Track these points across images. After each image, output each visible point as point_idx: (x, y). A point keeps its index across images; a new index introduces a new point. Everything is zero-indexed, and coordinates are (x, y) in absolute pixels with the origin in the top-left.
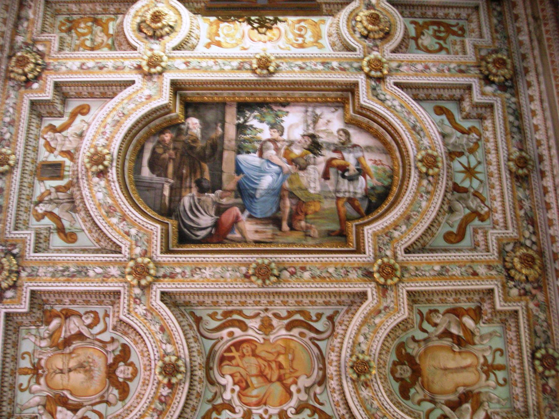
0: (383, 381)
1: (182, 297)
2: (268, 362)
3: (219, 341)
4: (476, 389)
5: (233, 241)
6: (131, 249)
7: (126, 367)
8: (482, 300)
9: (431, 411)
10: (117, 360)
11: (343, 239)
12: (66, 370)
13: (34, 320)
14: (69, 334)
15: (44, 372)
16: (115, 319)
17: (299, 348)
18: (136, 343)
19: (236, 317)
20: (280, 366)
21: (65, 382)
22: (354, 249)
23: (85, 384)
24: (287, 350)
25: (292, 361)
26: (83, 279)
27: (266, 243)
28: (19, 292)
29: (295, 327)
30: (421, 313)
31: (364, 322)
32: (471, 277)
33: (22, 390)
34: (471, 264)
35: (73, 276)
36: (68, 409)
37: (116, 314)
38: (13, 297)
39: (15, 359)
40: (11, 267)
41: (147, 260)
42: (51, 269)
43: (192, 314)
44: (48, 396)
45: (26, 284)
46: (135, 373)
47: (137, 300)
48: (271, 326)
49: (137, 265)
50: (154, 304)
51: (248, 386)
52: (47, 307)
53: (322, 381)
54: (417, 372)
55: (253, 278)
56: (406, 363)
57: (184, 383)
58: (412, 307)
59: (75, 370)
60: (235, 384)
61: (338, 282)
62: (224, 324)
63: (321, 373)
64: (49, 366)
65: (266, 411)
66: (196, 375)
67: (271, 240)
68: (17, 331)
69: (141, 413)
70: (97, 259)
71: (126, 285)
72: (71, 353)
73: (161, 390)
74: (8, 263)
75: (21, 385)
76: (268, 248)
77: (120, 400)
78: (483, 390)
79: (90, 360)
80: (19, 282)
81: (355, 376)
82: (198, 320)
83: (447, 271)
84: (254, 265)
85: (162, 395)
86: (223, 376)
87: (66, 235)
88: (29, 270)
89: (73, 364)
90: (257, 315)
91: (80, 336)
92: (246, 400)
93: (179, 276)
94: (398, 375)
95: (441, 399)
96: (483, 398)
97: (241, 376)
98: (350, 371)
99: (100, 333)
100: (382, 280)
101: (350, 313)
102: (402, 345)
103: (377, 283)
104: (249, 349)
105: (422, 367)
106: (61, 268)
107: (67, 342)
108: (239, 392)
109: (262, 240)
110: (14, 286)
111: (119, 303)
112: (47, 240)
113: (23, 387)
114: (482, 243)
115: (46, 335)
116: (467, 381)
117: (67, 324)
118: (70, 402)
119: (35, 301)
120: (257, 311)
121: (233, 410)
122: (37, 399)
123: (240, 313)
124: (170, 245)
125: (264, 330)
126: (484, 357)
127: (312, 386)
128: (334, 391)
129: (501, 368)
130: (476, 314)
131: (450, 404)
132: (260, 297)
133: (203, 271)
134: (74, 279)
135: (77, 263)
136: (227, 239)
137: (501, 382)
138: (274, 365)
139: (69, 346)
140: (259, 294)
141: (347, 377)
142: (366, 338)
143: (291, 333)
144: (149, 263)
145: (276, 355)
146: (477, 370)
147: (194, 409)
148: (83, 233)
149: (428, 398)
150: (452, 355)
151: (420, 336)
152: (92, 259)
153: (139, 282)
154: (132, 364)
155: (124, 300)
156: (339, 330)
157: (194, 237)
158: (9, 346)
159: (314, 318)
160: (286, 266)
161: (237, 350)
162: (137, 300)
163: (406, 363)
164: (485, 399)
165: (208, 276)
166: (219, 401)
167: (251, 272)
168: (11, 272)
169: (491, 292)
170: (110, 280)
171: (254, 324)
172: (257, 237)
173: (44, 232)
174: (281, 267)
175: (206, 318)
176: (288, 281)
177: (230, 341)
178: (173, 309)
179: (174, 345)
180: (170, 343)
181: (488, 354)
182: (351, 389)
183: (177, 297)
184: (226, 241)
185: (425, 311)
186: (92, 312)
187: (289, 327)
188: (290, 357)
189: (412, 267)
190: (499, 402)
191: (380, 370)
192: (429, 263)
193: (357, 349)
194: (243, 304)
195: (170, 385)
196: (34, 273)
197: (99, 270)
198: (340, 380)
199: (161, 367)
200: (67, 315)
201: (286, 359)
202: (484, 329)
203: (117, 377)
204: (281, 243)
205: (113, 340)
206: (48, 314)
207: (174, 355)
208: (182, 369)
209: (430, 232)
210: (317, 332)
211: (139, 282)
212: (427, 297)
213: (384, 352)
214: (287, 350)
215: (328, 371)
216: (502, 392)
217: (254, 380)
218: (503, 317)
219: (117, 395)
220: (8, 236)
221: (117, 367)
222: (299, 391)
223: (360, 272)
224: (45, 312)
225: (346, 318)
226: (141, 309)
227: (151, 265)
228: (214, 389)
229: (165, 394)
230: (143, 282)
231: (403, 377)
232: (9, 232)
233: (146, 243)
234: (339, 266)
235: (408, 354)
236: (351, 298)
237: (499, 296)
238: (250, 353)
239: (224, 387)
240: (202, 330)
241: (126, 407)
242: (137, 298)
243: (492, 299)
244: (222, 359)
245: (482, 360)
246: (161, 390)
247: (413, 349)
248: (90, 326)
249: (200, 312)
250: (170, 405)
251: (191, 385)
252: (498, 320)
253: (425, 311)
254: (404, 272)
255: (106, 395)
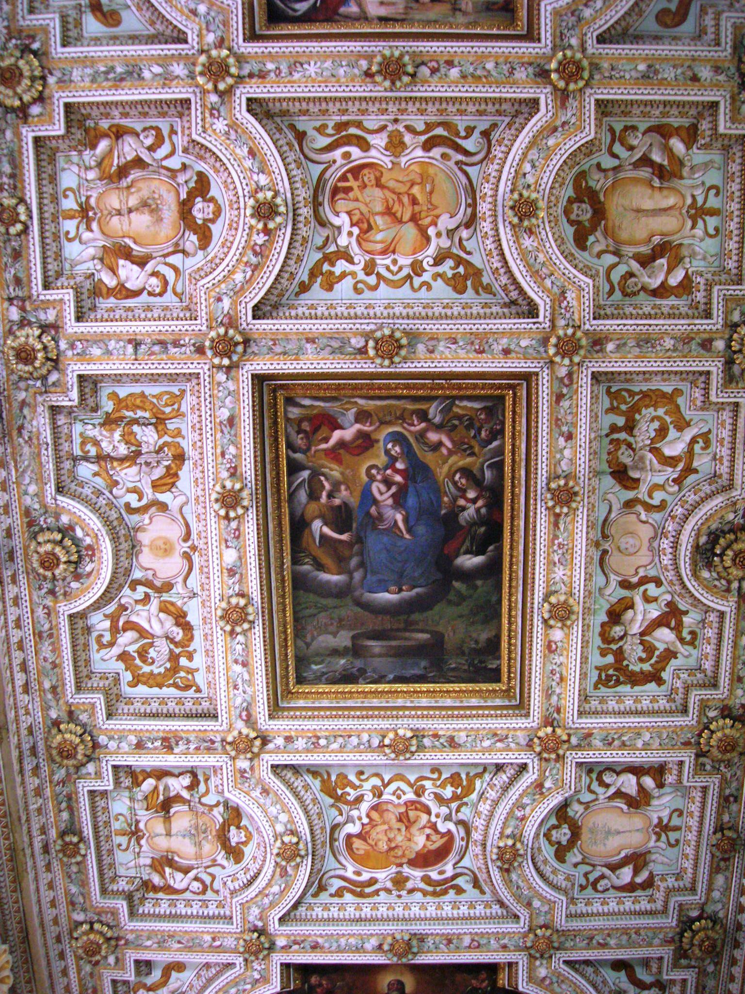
0: (553, 224)
1: (278, 104)
2: (399, 194)
3: (330, 166)
4: (676, 239)
5: (348, 18)
6: (200, 36)
7: (206, 204)
8: (700, 116)
9: (614, 266)
10: (192, 195)
11: (509, 15)
12: (125, 211)
13: (74, 144)
14: (123, 161)
15: (95, 214)
16: (186, 139)
17: (440, 179)
18: (217, 171)
19: (353, 131)
20: (414, 201)
21: (126, 227)
22: (525, 33)
23: (152, 229)
24: (424, 178)
25: (431, 193)
26: (137, 83)
27: (396, 20)
28: (48, 108)
29: (435, 146)
30: (612, 130)
31: (532, 144)
32: (689, 83)
33: (70, 240)
34: (692, 64)
35: (122, 80)
36: (133, 263)
37: (187, 132)
38: (41, 114)
39: (55, 200)
40: (32, 71)
41: (225, 52)
42: (89, 71)
43: (292, 127)
44: (104, 247)
45: (57, 96)
46: (218, 212)
47: (215, 112)
48: (402, 145)
49: (211, 62)
50: (238, 116)
51: (370, 228)
52: (90, 123)
53: (471, 222)
54: (599, 213)
55: (378, 79)
56: (586, 199)
57: (285, 227)
58: (601, 120)
59: (137, 209)
60: (352, 225)
61: (498, 84)
62: (336, 140)
63: (469, 211)
64: (102, 206)
65: (395, 262)
66: (300, 215)
67: (404, 17)
68: (52, 160)
69: (230, 268)
70: (153, 52)
71: (197, 91)
72: (128, 188)
73: (255, 237)
74: (28, 67)
75: (68, 233)
76: (398, 30)
77: (200, 249)
78: (686, 242)
79: (156, 196)
80: (47, 93)
81: (516, 220)
82: (301, 136)
83: (656, 72)
84: (379, 59)
85: (256, 244)
86: (337, 214)
87: (104, 15)
88: (58, 74)
89: (133, 201)
90: (383, 128)
91: (138, 163)
92: (370, 246)
93: (272, 75)
94: (573, 217)
95: (629, 250)
96: (685, 252)
97: (362, 214)
98: (510, 213)
99: (166, 157)
100: (561, 84)
101: (513, 128)
102: (582, 175)
103: (555, 88)
104: (372, 177)
105: (607, 207)
106: (103, 69)
107: (123, 171)
108: (358, 236)
109: (390, 16)
110: (41, 99)
111: (189, 115)
112: (78, 24)
113: (70, 236)
114: (711, 30)
115: (93, 164)
116: (665, 230)
117: (120, 146)
118: (134, 253)
119: (73, 117)
120: (383, 123)
121: (350, 260)
122: (91, 251)
123: (359, 125)
124: (257, 27)
125: (392, 149)
126: (693, 197)
127: (457, 227)
128: (485, 236)
129: (713, 212)
130: (689, 134)
131: (637, 258)
132: (387, 104)
133: (306, 66)
134: (124, 84)
135: (126, 60)
136: (338, 14)
137: (711, 231)
138: (405, 200)
139: (126, 177)
140: (386, 99)
141: (504, 221)
142: (533, 166)
143: (431, 154)
144: (228, 56)
145: (409, 185)
146: (680, 214)
147: (299, 260)
148: (129, 11)
149: (611, 249)
150: (650, 191)
151: (608, 162)
152: (146, 52)
153: (216, 87)
154: (212, 200)
155: (195, 112)
156: (497, 151)
157: (291, 13)
158: (44, 182)
159: (463, 134)
160: (426, 59)
161: (356, 178)
162: (214, 112)
163: (586, 199)
164: (686, 254)
165: (313, 75)
166: (332, 248)
167: (374, 68)
168: (33, 79)
169: (714, 105)
170: (175, 82)
171: (379, 141)
172: (383, 12)
173: (73, 13)
174: (419, 60)
175: (311, 133)
176: (427, 82)
177: (345, 165)
178: (265, 121)
179: (270, 175)
180: (263, 173)
181: (699, 192)
182: (509, 237)
183: (271, 105)
184: (337, 17)
185: (618, 127)
186: (152, 128)
187: (428, 146)
188: (428, 188)
189: (606, 65)
190: (704, 259)
191: (551, 211)
192: (632, 59)
193: (521, 182)
194: (364, 112)
195: (266, 231)
196: (66, 78)
197: (157, 69)
198: (495, 222)
199: (253, 208)
200: (119, 133)
201: (423, 190)
202: (698, 156)
203: (194, 218)
204: (418, 22)
205: (184, 167)
206: (92, 133)
207: (269, 189)
208: (282, 209)
209: (637, 9)
210: (466, 153)
211: (216, 87)
212: (623, 108)
213: (557, 185)
214: (424, 178)
215: (479, 208)
216: (711, 246)
217: (379, 221)
218: (726, 142)
219: (197, 243)
220: (22, 23)
221: (193, 205)
222: (439, 235)
223: (530, 70)
224: (87, 131)
225: (508, 135)
226: (220, 125)
227: (231, 61)
228: (325, 232)
229: (260, 242)
230: (222, 86)
231: (580, 219)
232: (23, 17)
233: (221, 26)
234: (501, 60)
235: (589, 189)
236: (516, 106)
237: (725, 114)
238: (373, 182)
239: (339, 228)
240: (306, 150)
241: (209, 258)
242: (213, 108)
243: (715, 115)
244: (335, 191)
245: (689, 201)
246: (255, 237)
247: (597, 181)
248: (151, 149)
249: (304, 124)
250: (268, 257)
251: (293, 229)
252: (719, 146)
253: (618, 127)
254: (595, 72)
255: (181, 242)
